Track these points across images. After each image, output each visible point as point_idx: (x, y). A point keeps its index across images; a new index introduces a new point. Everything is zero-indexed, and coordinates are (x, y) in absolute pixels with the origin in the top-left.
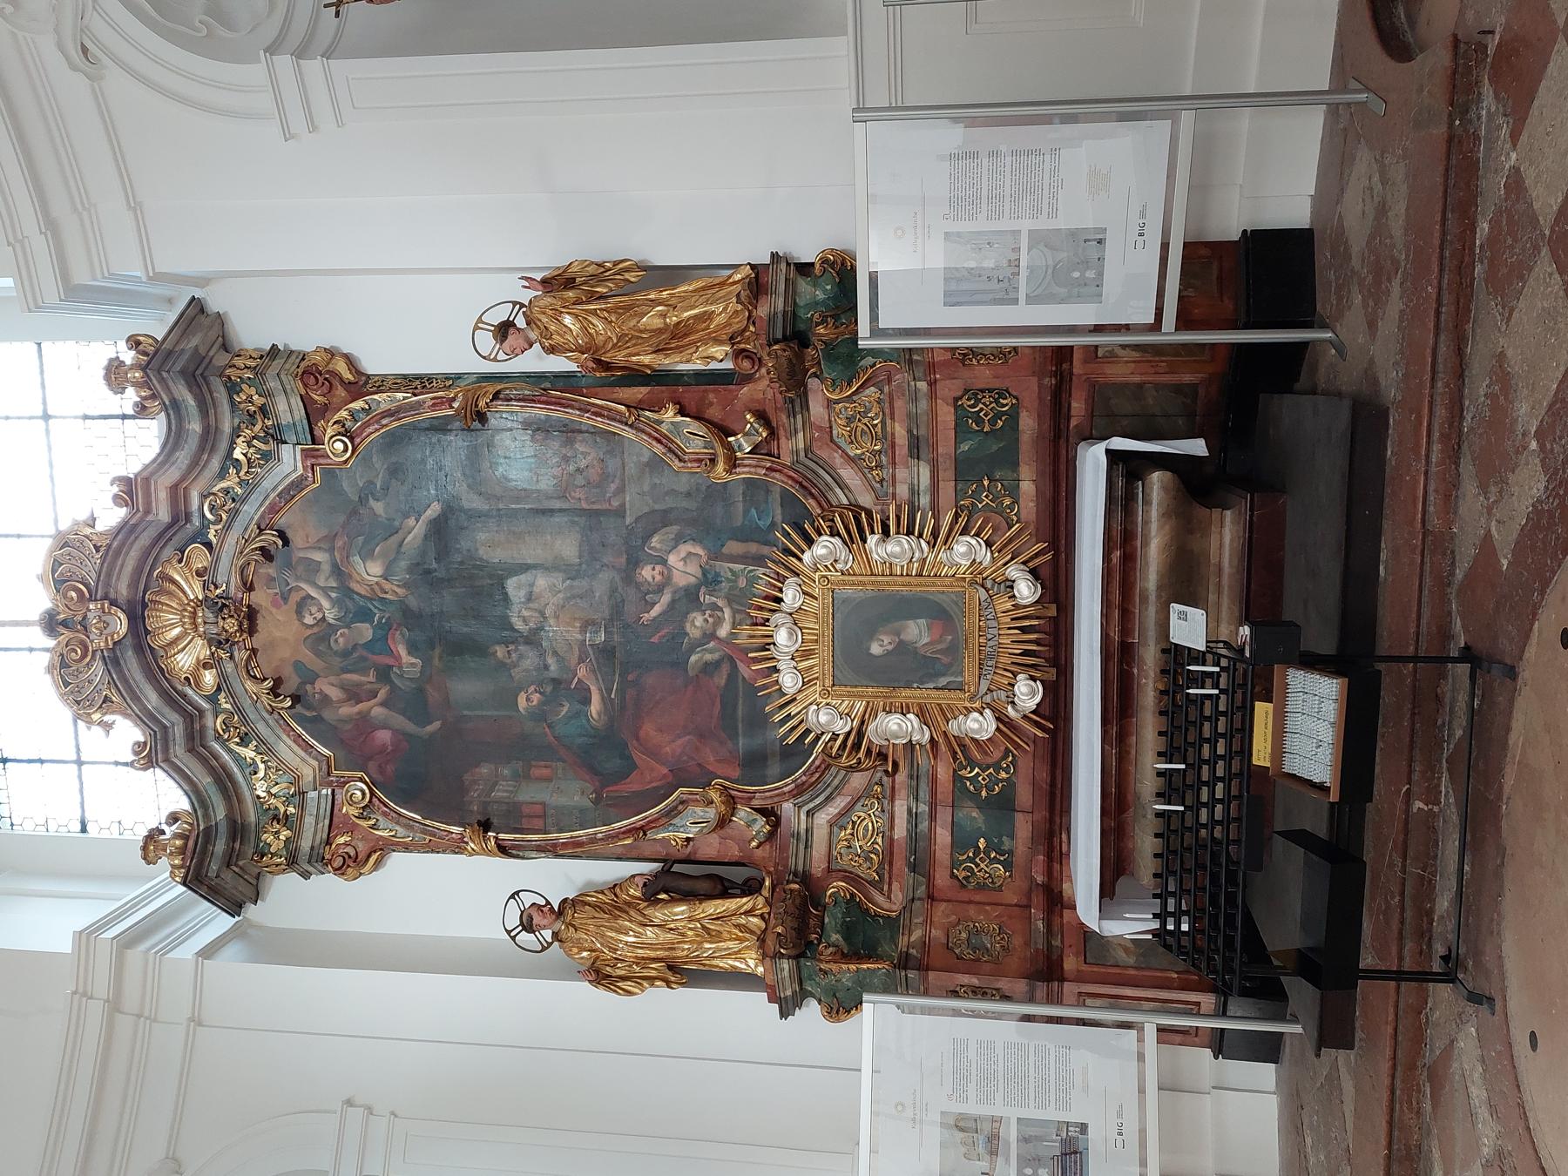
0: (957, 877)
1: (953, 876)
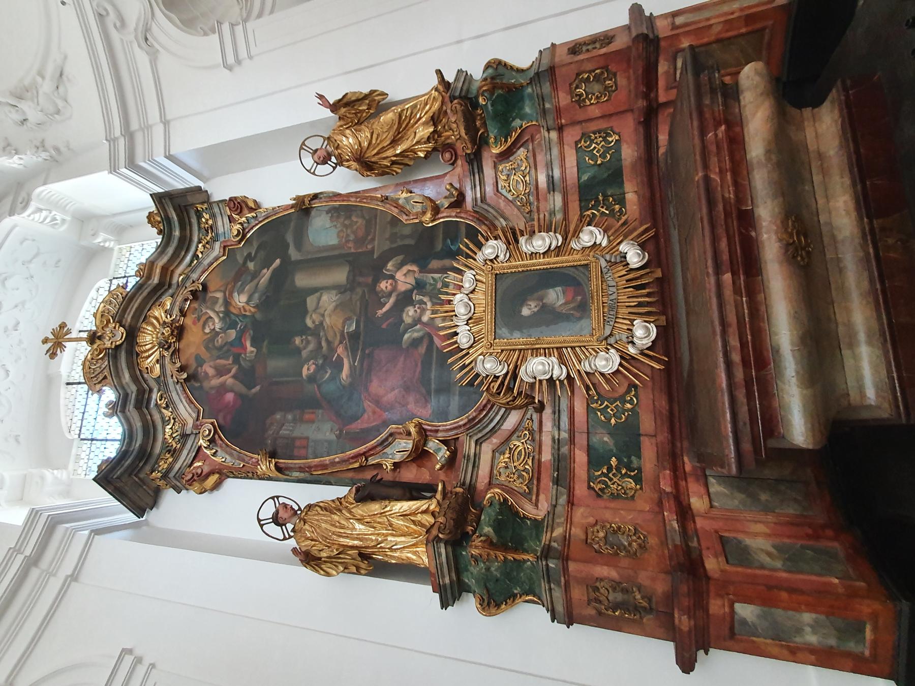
0: (593, 489)
1: (589, 487)
